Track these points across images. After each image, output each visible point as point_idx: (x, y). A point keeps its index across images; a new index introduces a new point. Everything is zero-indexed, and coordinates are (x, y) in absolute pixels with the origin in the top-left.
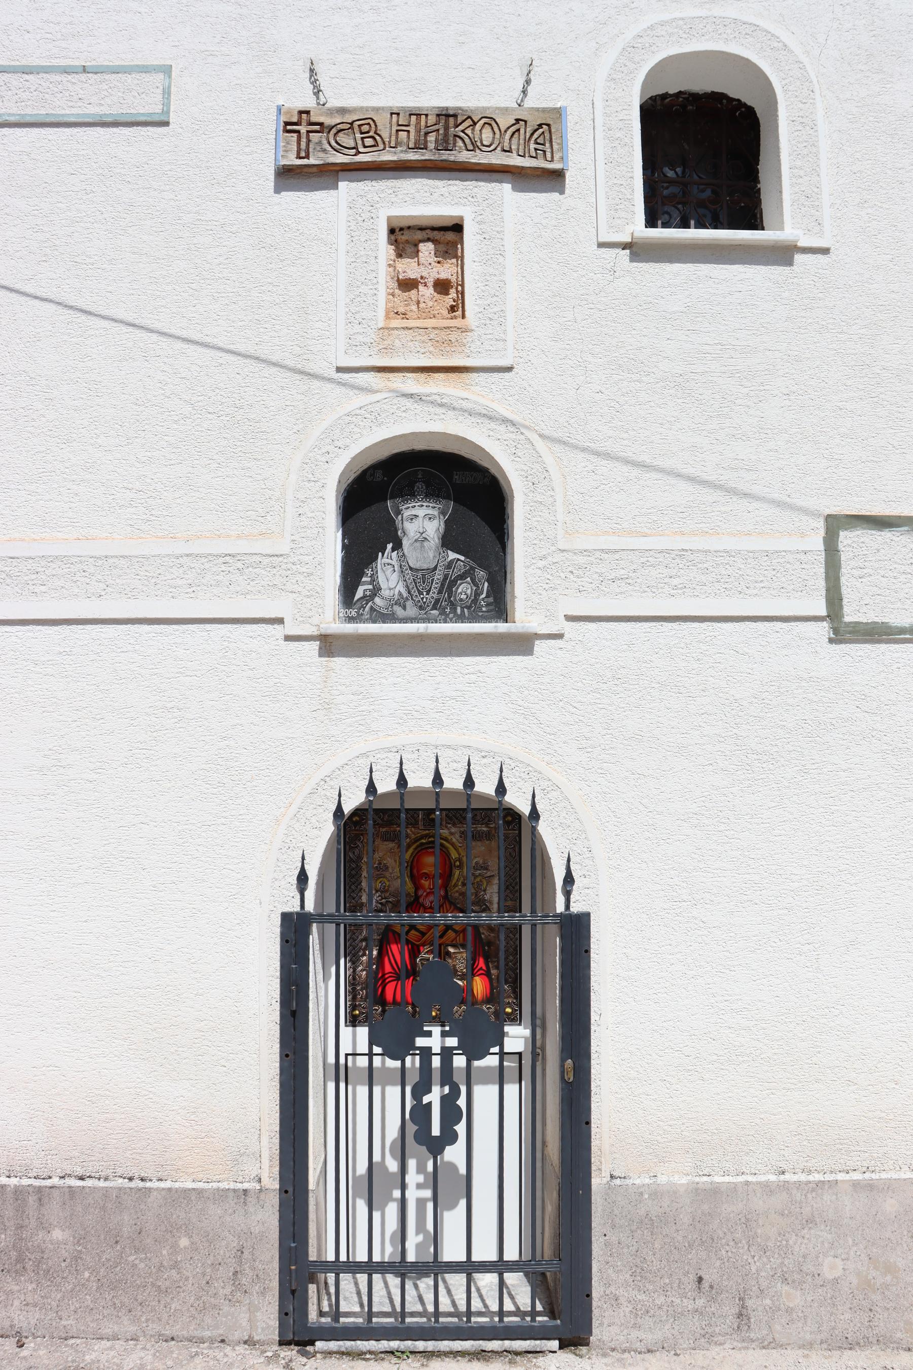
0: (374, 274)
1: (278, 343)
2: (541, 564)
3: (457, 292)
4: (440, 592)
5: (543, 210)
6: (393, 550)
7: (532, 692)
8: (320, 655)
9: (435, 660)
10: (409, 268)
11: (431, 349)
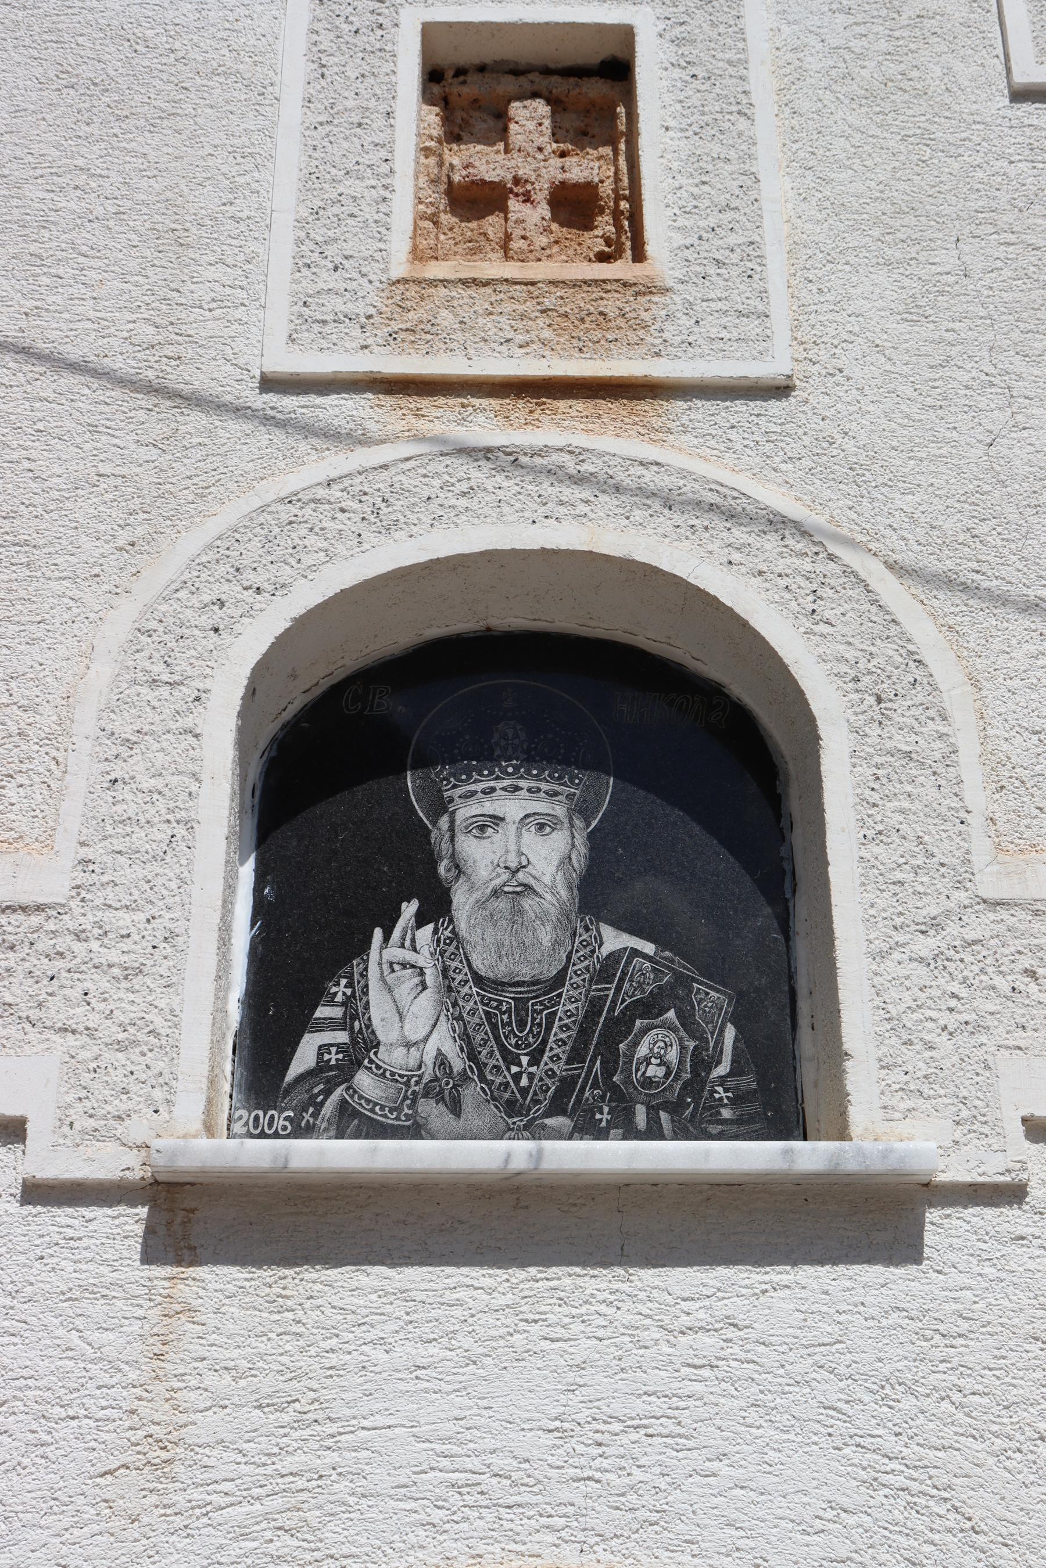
0: (383, 154)
1: (92, 314)
2: (925, 946)
3: (617, 214)
4: (576, 1056)
5: (851, 20)
6: (421, 920)
7: (928, 1403)
8: (148, 1258)
9: (566, 1278)
10: (486, 163)
11: (547, 334)
